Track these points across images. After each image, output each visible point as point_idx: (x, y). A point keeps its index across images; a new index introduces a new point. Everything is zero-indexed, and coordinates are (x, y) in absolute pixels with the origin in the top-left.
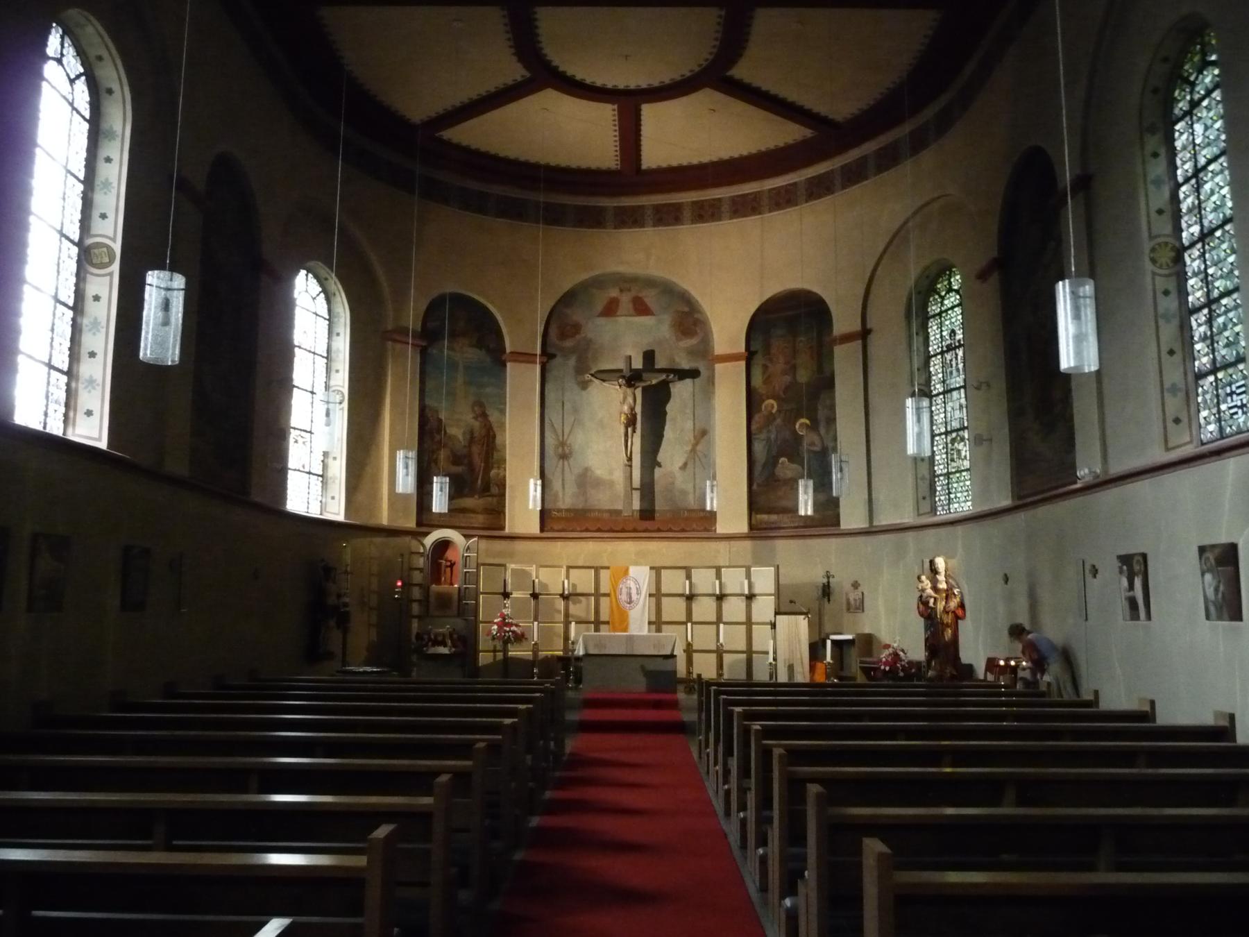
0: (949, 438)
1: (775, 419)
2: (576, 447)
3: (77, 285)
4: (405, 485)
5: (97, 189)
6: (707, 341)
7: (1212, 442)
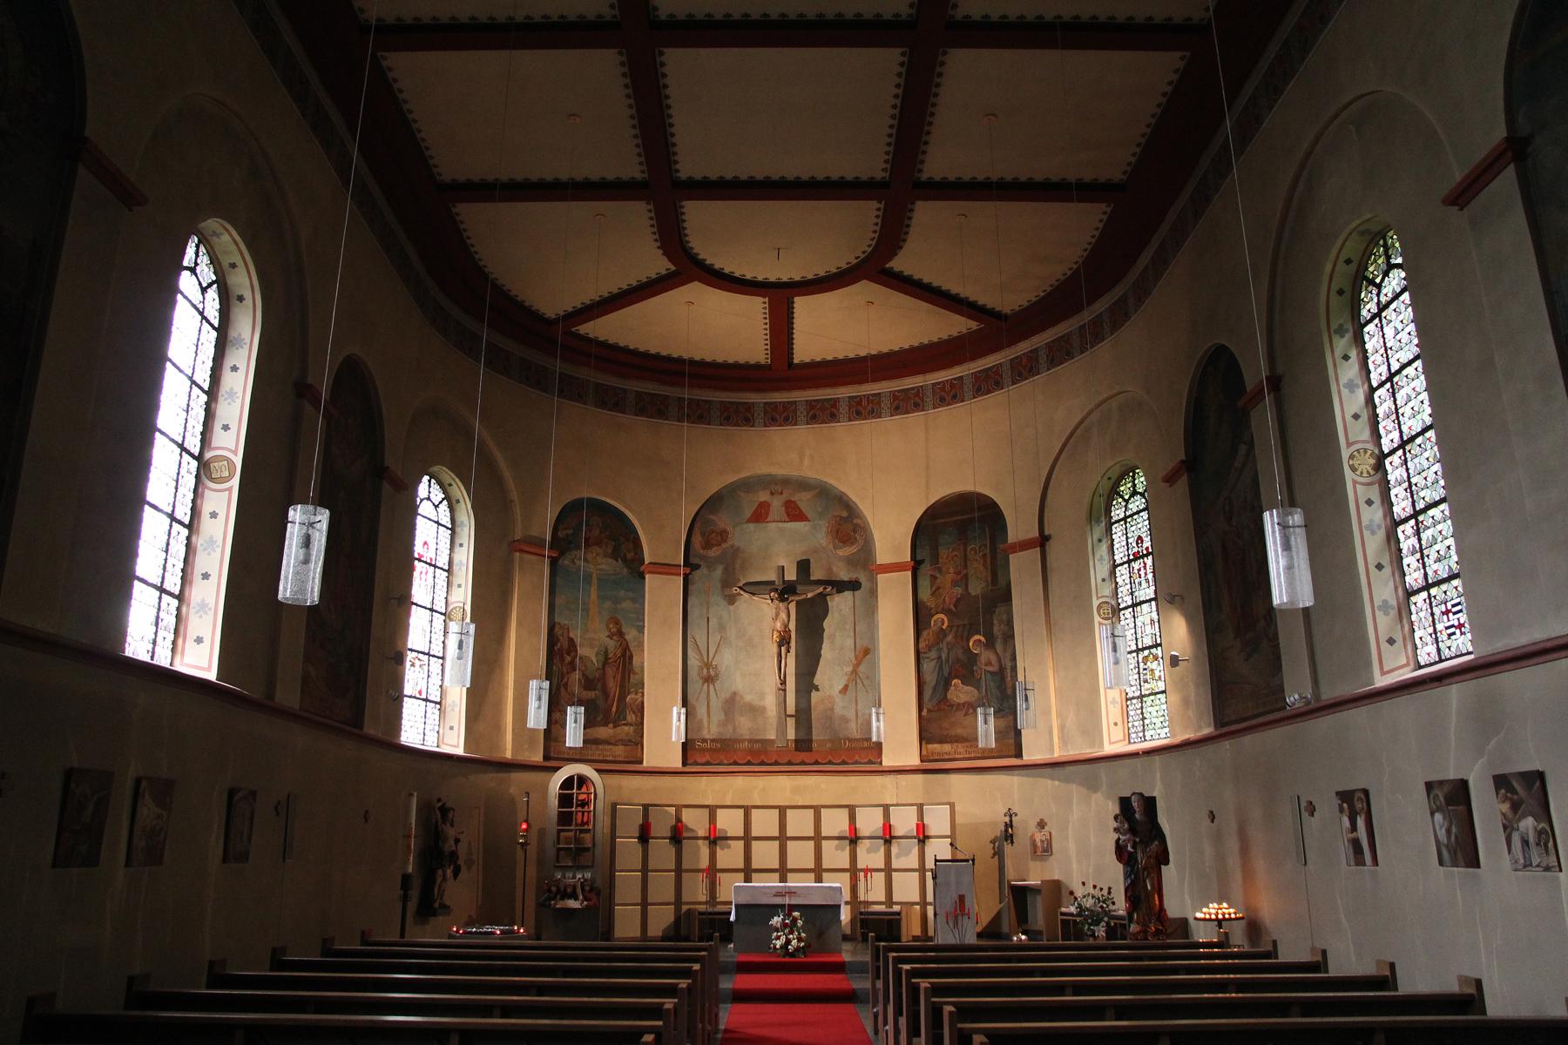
0: (1141, 657)
1: (945, 636)
2: (722, 669)
3: (194, 501)
4: (537, 718)
5: (221, 399)
6: (868, 549)
7: (1431, 664)
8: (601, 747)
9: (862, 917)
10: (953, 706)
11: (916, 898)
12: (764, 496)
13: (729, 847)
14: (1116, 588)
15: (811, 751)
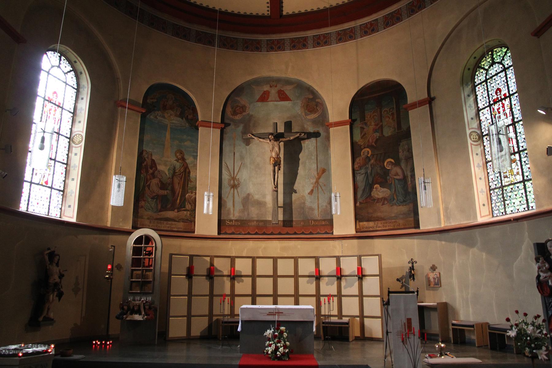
0: (500, 161)
1: (370, 160)
2: (242, 181)
8: (170, 222)
9: (324, 325)
10: (374, 200)
11: (357, 313)
12: (266, 88)
13: (242, 281)
14: (480, 124)
15: (292, 227)
